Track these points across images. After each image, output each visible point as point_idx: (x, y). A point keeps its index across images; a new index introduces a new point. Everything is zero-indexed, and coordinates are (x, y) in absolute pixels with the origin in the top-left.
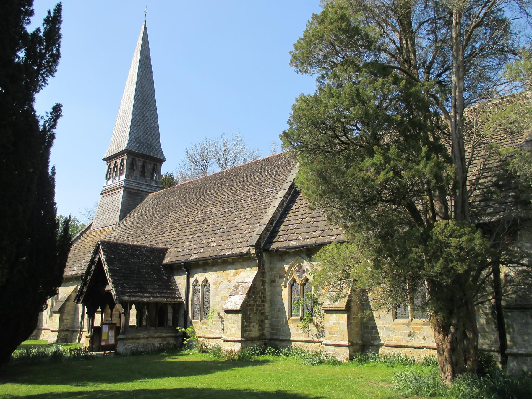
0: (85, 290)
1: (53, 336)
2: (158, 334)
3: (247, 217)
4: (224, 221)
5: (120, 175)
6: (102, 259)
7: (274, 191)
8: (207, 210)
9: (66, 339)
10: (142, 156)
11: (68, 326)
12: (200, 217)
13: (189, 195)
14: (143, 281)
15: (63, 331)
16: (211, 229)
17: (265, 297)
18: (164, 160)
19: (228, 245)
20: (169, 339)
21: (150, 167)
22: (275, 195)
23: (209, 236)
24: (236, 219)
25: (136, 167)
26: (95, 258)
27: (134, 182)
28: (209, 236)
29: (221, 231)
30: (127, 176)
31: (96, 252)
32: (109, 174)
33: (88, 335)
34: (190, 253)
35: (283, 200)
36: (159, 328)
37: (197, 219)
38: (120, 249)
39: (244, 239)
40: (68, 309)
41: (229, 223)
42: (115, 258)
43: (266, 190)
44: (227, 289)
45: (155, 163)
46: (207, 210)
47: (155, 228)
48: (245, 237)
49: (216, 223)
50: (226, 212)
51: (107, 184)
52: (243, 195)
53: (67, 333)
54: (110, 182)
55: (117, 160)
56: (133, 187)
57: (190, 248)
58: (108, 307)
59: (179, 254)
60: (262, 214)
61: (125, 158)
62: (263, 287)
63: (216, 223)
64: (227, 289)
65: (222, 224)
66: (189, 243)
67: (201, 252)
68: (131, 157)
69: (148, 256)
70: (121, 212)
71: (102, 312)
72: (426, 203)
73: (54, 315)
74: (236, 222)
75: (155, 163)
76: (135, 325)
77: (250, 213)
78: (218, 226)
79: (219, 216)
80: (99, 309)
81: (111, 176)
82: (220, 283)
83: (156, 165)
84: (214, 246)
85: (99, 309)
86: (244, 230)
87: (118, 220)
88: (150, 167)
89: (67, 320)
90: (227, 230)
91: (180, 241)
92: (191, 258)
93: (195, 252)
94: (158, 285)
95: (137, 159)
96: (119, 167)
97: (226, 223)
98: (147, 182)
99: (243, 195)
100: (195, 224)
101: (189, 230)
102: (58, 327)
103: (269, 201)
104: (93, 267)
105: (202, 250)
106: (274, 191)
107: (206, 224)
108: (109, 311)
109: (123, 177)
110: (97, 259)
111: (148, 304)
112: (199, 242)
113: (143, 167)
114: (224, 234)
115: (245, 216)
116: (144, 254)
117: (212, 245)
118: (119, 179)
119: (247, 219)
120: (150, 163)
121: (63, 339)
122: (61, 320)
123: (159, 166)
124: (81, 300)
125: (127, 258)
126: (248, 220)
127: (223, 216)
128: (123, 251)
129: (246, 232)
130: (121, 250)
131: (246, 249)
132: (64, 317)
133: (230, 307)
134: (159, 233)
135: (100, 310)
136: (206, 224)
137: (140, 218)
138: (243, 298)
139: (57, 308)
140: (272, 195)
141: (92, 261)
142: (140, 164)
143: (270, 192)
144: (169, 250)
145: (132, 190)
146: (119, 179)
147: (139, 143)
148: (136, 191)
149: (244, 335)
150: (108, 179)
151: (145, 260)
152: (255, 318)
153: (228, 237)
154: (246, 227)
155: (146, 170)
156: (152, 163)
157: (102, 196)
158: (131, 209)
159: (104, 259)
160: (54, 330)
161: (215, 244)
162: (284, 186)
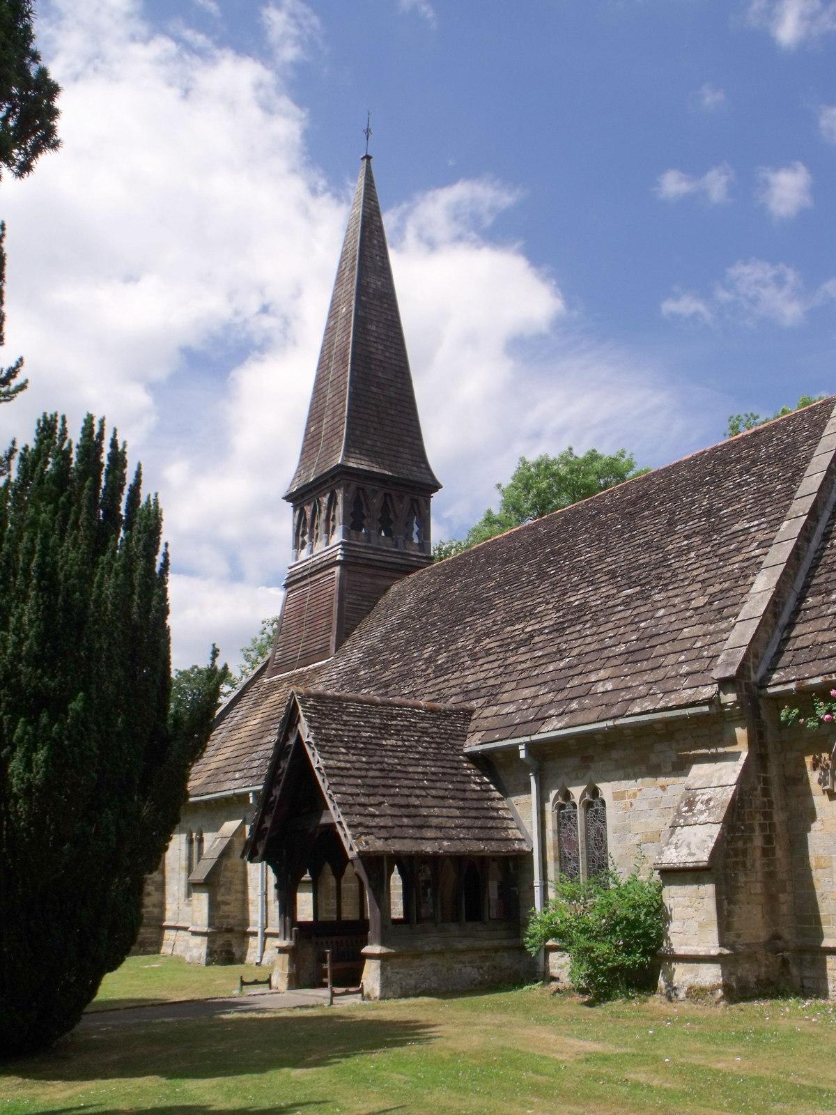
0: (268, 824)
1: (197, 946)
3: (694, 604)
4: (629, 621)
5: (329, 531)
6: (305, 739)
7: (763, 526)
8: (572, 599)
11: (232, 921)
12: (551, 619)
13: (513, 566)
16: (593, 647)
17: (772, 826)
18: (436, 487)
19: (650, 685)
22: (767, 537)
23: (591, 667)
24: (661, 612)
25: (369, 510)
26: (286, 739)
28: (591, 667)
29: (622, 648)
30: (346, 534)
31: (290, 721)
32: (304, 531)
33: (285, 943)
34: (539, 716)
35: (796, 547)
36: (470, 925)
37: (545, 624)
39: (696, 666)
40: (225, 876)
41: (642, 625)
43: (737, 527)
44: (656, 811)
46: (572, 599)
47: (430, 660)
48: (699, 658)
49: (601, 629)
50: (628, 596)
51: (297, 558)
52: (670, 547)
53: (228, 936)
54: (304, 554)
57: (538, 702)
58: (327, 868)
59: (507, 721)
60: (739, 590)
62: (765, 799)
63: (601, 629)
64: (656, 811)
65: (622, 630)
66: (533, 689)
67: (572, 712)
71: (316, 887)
73: (195, 895)
74: (665, 620)
76: (402, 916)
77: (702, 591)
78: (610, 637)
79: (609, 611)
80: (307, 877)
81: (306, 538)
82: (635, 795)
83: (417, 501)
84: (607, 692)
85: (307, 877)
86: (693, 640)
90: (640, 645)
91: (507, 687)
93: (552, 712)
97: (634, 627)
98: (396, 546)
99: (670, 547)
100: (542, 638)
101: (528, 656)
103: (753, 554)
104: (285, 765)
105: (574, 705)
106: (763, 526)
107: (575, 636)
108: (332, 881)
109: (337, 538)
110: (292, 741)
111: (434, 859)
112: (561, 684)
113: (385, 509)
114: (631, 656)
115: (689, 601)
117: (601, 689)
119: (696, 609)
121: (221, 952)
122: (213, 905)
124: (261, 851)
126: (699, 611)
127: (620, 608)
129: (699, 644)
131: (708, 692)
132: (219, 898)
133: (674, 857)
134: (441, 671)
135: (310, 879)
136: (575, 636)
138: (716, 830)
139: (201, 873)
140: (760, 536)
141: (281, 749)
142: (377, 502)
143: (753, 530)
144: (478, 712)
149: (725, 940)
150: (298, 545)
152: (752, 885)
153: (645, 663)
154: (697, 630)
157: (289, 589)
158: (239, 887)
159: (310, 740)
160: (198, 929)
161: (609, 686)
162: (793, 508)
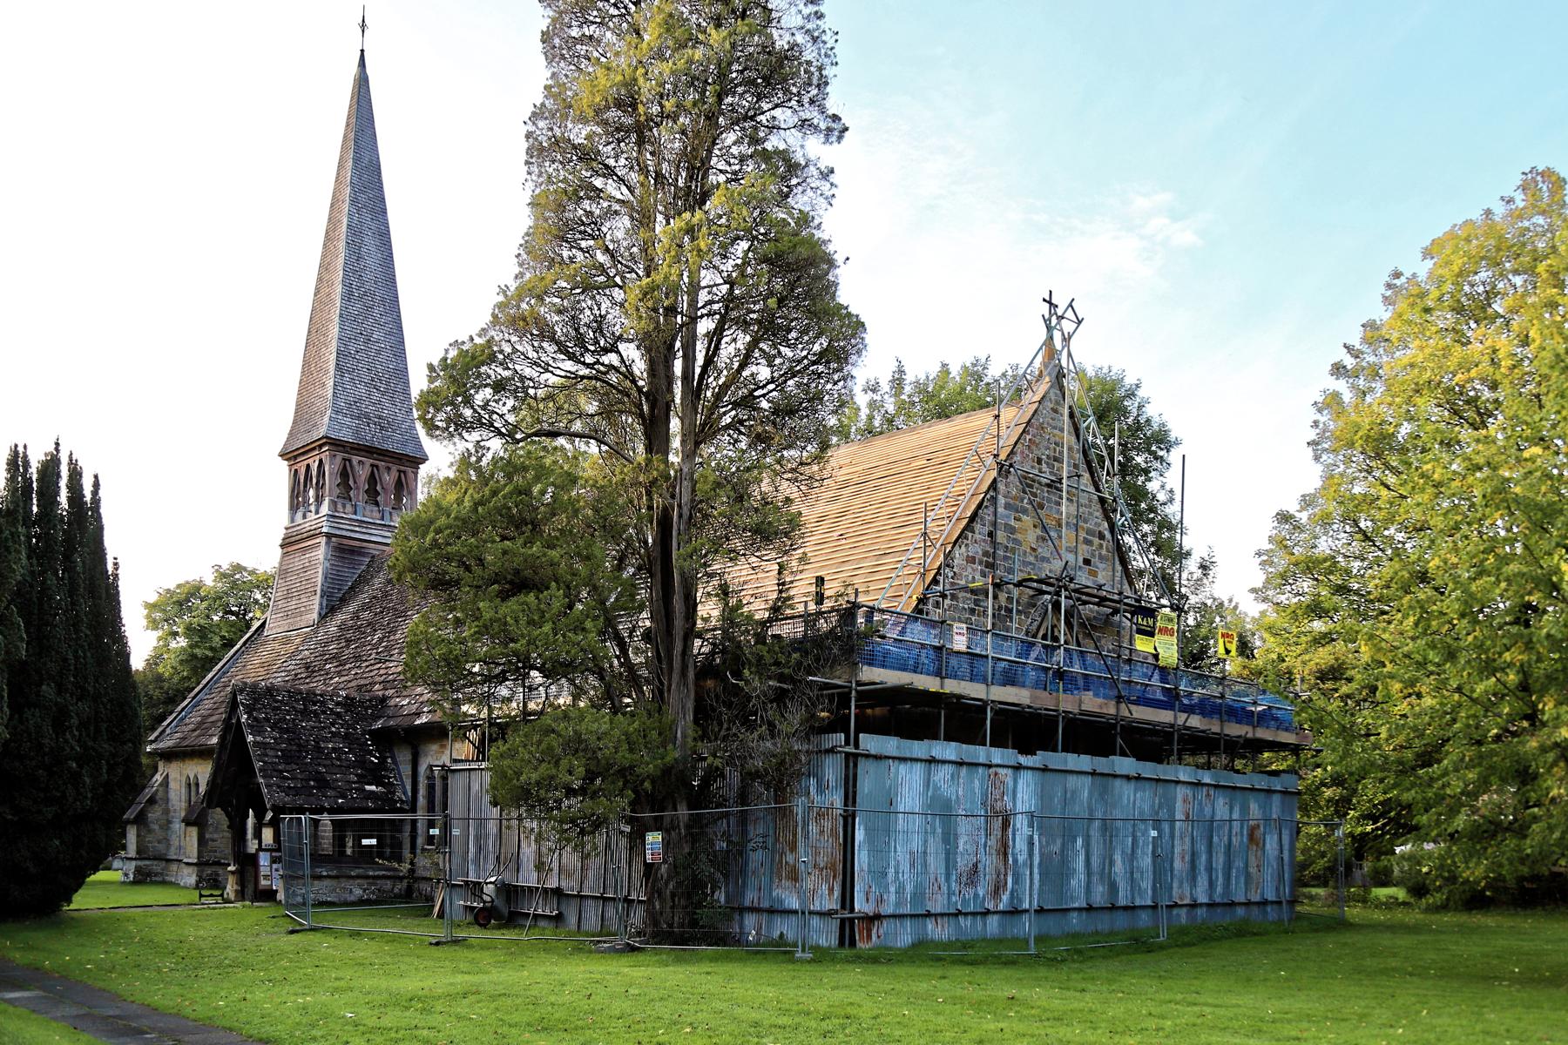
2: (360, 871)
9: (216, 880)
10: (369, 451)
14: (325, 766)
15: (207, 864)
20: (383, 881)
21: (389, 479)
27: (350, 519)
32: (297, 501)
38: (278, 701)
42: (267, 720)
45: (402, 468)
55: (310, 461)
56: (348, 534)
61: (325, 457)
68: (340, 456)
69: (339, 715)
70: (322, 597)
72: (1139, 517)
75: (402, 468)
83: (404, 472)
87: (315, 616)
88: (389, 479)
89: (213, 840)
92: (418, 722)
94: (357, 775)
95: (355, 459)
96: (314, 481)
102: (196, 855)
113: (372, 480)
116: (331, 710)
118: (317, 513)
120: (389, 469)
123: (411, 475)
125: (294, 720)
128: (286, 705)
130: (281, 701)
137: (356, 616)
142: (363, 473)
145: (345, 542)
146: (317, 513)
147: (359, 418)
148: (357, 544)
151: (333, 724)
155: (379, 488)
156: (394, 468)
160: (190, 861)
